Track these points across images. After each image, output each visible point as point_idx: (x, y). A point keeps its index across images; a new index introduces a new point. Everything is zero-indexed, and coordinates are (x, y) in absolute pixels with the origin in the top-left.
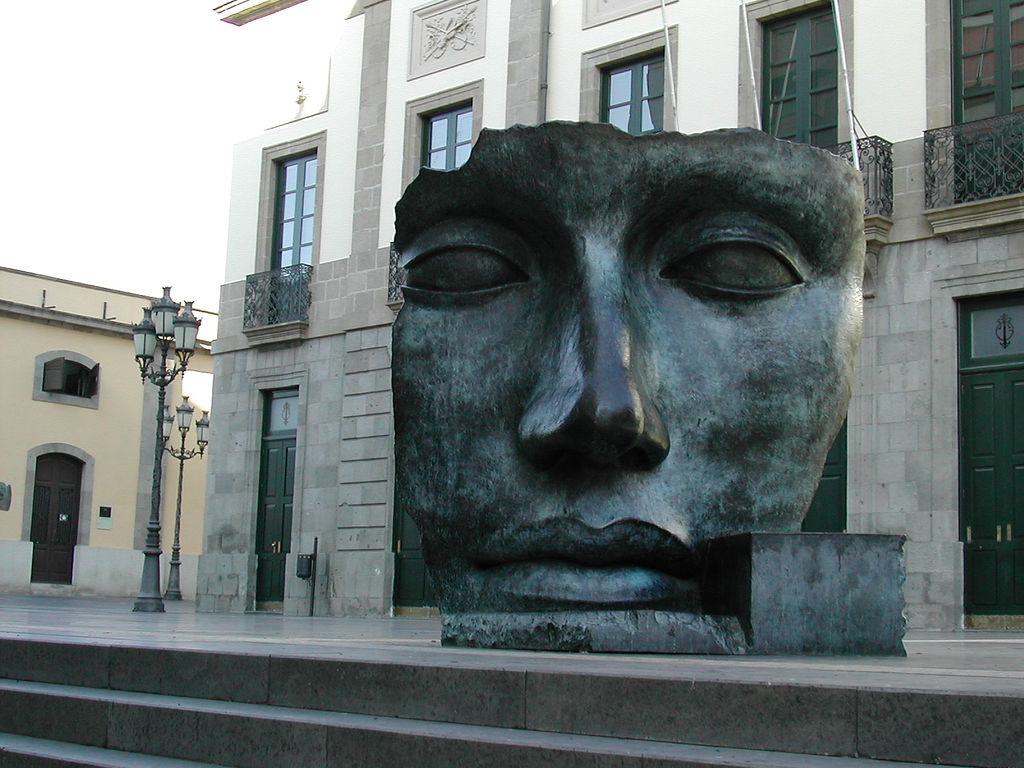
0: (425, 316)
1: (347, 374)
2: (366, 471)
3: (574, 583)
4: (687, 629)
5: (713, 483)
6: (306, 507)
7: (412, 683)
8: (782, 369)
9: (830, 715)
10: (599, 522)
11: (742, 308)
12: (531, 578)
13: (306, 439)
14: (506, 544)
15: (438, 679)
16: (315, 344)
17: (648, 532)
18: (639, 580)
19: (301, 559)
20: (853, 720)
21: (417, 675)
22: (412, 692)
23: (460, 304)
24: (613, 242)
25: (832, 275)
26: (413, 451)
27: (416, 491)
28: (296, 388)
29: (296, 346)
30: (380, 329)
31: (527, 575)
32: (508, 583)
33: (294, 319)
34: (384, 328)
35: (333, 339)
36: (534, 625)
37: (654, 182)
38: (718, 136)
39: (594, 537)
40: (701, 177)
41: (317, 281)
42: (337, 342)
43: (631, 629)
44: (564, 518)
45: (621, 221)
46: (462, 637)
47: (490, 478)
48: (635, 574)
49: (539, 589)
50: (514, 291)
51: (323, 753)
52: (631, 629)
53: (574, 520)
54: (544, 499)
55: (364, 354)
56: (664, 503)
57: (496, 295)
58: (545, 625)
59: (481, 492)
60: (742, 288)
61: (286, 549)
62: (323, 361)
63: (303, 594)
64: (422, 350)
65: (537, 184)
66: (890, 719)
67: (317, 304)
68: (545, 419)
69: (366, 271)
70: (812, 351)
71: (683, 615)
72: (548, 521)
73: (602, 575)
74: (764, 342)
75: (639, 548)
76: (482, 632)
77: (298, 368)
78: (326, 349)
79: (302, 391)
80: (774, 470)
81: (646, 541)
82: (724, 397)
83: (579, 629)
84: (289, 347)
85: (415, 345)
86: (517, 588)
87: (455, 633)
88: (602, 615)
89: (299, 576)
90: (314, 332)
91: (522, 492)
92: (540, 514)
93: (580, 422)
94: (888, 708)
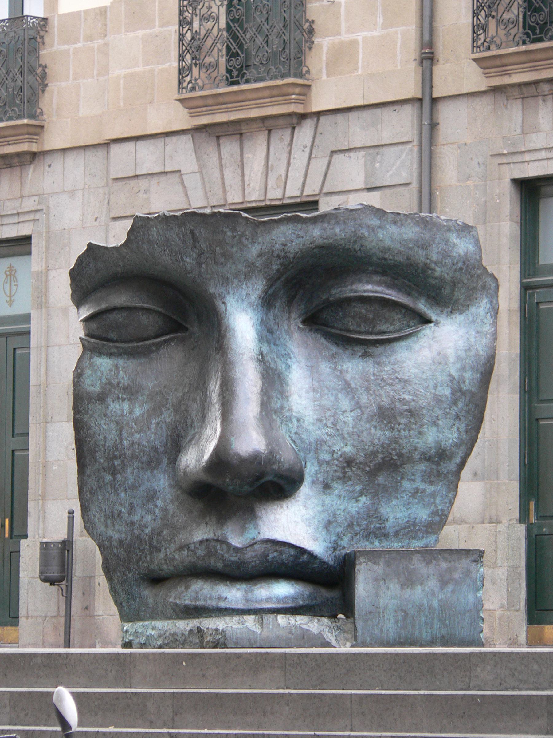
0: (104, 364)
1: (115, 219)
2: (254, 389)
3: (233, 594)
4: (303, 628)
5: (347, 503)
6: (51, 458)
7: (65, 665)
8: (409, 402)
9: (274, 667)
10: (236, 541)
11: (370, 350)
12: (190, 590)
13: (47, 334)
14: (170, 563)
15: (81, 661)
16: (57, 162)
17: (286, 549)
18: (283, 590)
19: (45, 547)
20: (284, 669)
21: (68, 660)
22: (66, 670)
23: (131, 354)
24: (251, 305)
25: (461, 314)
26: (92, 482)
27: (97, 517)
28: (26, 240)
29: (22, 165)
30: (168, 139)
31: (187, 588)
32: (173, 594)
33: (19, 117)
34: (174, 139)
35: (89, 153)
36: (188, 629)
37: (282, 254)
38: (333, 214)
39: (239, 555)
40: (322, 247)
41: (55, 50)
42: (95, 158)
43: (257, 629)
44: (214, 540)
45: (256, 288)
46: (137, 641)
47: (156, 506)
48: (278, 584)
49: (197, 599)
50: (176, 341)
51: (8, 709)
52: (257, 629)
53: (223, 542)
54: (198, 525)
55: (143, 184)
56: (294, 523)
57: (158, 346)
58: (195, 628)
59: (149, 518)
60: (371, 333)
61: (19, 532)
62: (72, 193)
63: (53, 611)
64: (98, 394)
65: (183, 261)
66: (299, 668)
67: (56, 87)
68: (196, 457)
69: (140, 33)
70: (439, 385)
71: (302, 617)
72: (201, 542)
73: (249, 586)
74: (393, 379)
75: (291, 564)
76: (149, 637)
77: (29, 204)
78: (75, 169)
79: (36, 246)
80: (404, 491)
81: (284, 557)
82: (355, 430)
83: (217, 630)
84: (10, 166)
85: (91, 389)
86: (180, 598)
87: (131, 638)
88: (236, 618)
89: (45, 580)
90: (54, 140)
91: (181, 518)
92: (194, 537)
93: (220, 462)
94: (298, 662)
